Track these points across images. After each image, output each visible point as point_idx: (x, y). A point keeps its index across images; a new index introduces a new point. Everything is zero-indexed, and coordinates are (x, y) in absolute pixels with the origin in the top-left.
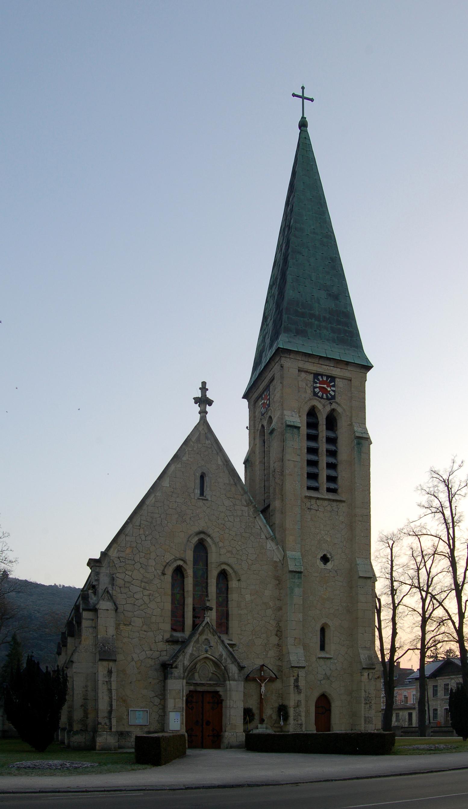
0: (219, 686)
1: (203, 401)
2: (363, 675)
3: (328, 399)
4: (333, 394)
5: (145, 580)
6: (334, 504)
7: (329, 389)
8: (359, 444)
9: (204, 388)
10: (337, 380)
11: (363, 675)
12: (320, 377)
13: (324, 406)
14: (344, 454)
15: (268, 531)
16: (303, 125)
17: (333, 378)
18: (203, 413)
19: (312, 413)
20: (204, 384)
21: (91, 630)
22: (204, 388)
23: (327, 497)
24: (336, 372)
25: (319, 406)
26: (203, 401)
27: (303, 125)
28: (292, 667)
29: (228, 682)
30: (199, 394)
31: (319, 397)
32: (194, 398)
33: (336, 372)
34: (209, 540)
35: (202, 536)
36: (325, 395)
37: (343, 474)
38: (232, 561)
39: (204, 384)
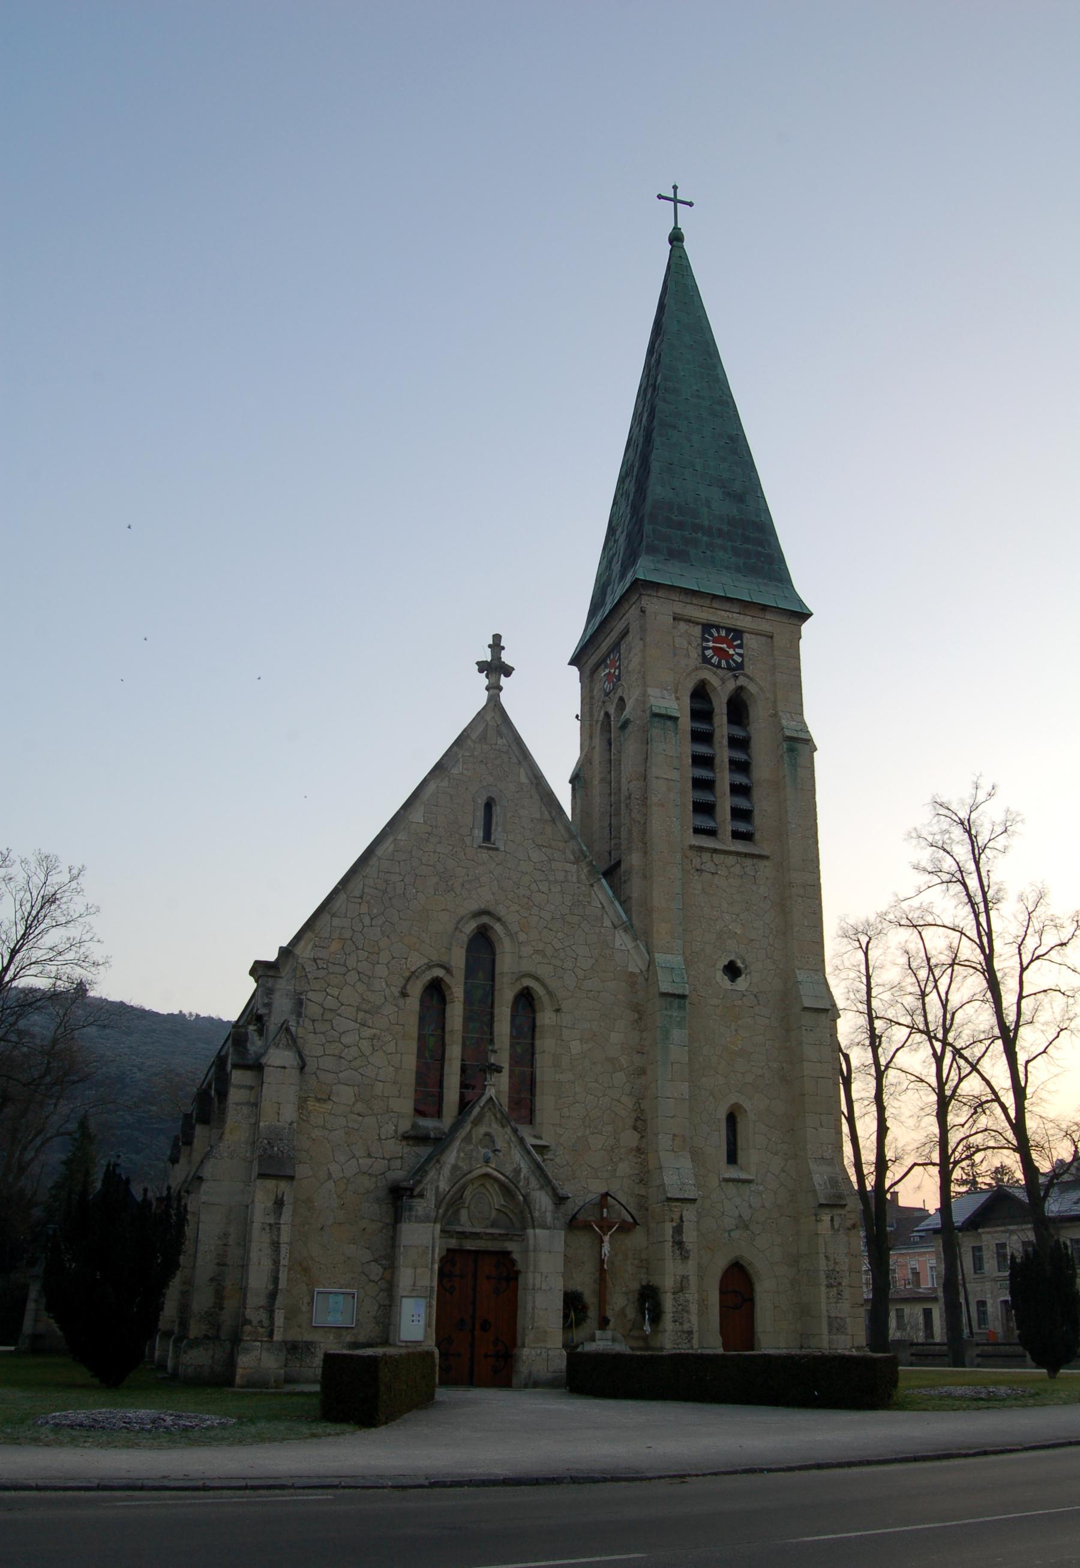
0: (511, 1240)
1: (495, 668)
2: (820, 1221)
3: (729, 668)
4: (739, 660)
5: (365, 1006)
6: (748, 862)
7: (731, 652)
8: (791, 750)
9: (496, 645)
10: (746, 636)
11: (820, 1221)
12: (714, 631)
13: (723, 681)
14: (763, 766)
15: (616, 911)
16: (676, 238)
17: (738, 633)
18: (494, 689)
19: (701, 693)
20: (497, 638)
21: (245, 1110)
22: (496, 645)
23: (732, 848)
24: (743, 621)
25: (715, 681)
26: (495, 668)
27: (676, 238)
28: (669, 1199)
29: (530, 1231)
30: (487, 656)
31: (713, 665)
32: (478, 663)
33: (743, 621)
34: (498, 927)
35: (485, 919)
36: (723, 663)
37: (763, 805)
38: (542, 971)
39: (497, 638)
